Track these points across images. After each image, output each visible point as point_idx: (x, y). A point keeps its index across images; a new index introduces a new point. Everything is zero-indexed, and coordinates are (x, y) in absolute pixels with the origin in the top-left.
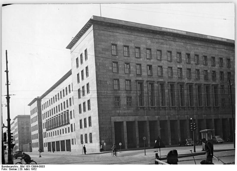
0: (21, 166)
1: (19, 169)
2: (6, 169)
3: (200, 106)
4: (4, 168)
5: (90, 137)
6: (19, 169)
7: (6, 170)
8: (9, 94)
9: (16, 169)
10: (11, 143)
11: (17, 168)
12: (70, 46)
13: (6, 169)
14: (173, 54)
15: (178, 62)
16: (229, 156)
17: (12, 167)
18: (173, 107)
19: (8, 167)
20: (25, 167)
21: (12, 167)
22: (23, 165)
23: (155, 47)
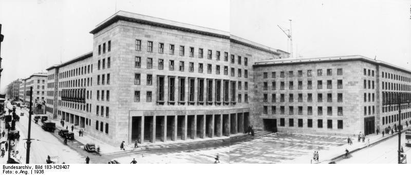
1: (33, 172)
2: (11, 172)
4: (7, 170)
5: (163, 92)
6: (33, 172)
7: (10, 174)
8: (31, 138)
12: (95, 32)
13: (11, 172)
16: (366, 147)
17: (20, 168)
19: (14, 167)
21: (20, 168)
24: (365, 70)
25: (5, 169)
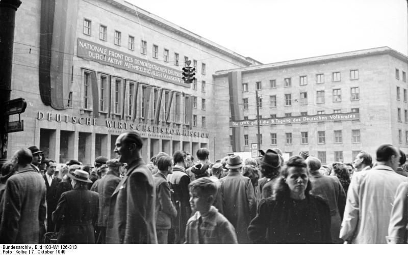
0: (36, 247)
3: (102, 110)
4: (7, 250)
7: (10, 254)
9: (25, 252)
10: (198, 202)
11: (27, 250)
13: (11, 252)
14: (136, 41)
15: (84, 34)
17: (20, 248)
18: (86, 109)
19: (14, 247)
20: (43, 247)
21: (20, 248)
22: (40, 245)
23: (126, 32)
24: (397, 71)
25: (5, 249)
